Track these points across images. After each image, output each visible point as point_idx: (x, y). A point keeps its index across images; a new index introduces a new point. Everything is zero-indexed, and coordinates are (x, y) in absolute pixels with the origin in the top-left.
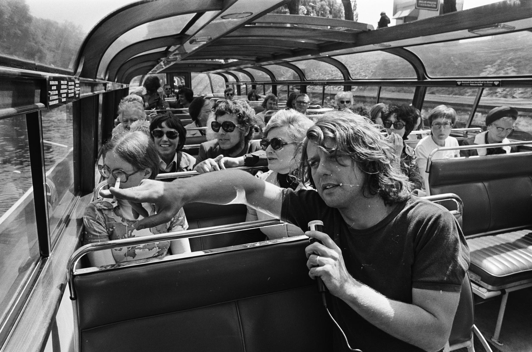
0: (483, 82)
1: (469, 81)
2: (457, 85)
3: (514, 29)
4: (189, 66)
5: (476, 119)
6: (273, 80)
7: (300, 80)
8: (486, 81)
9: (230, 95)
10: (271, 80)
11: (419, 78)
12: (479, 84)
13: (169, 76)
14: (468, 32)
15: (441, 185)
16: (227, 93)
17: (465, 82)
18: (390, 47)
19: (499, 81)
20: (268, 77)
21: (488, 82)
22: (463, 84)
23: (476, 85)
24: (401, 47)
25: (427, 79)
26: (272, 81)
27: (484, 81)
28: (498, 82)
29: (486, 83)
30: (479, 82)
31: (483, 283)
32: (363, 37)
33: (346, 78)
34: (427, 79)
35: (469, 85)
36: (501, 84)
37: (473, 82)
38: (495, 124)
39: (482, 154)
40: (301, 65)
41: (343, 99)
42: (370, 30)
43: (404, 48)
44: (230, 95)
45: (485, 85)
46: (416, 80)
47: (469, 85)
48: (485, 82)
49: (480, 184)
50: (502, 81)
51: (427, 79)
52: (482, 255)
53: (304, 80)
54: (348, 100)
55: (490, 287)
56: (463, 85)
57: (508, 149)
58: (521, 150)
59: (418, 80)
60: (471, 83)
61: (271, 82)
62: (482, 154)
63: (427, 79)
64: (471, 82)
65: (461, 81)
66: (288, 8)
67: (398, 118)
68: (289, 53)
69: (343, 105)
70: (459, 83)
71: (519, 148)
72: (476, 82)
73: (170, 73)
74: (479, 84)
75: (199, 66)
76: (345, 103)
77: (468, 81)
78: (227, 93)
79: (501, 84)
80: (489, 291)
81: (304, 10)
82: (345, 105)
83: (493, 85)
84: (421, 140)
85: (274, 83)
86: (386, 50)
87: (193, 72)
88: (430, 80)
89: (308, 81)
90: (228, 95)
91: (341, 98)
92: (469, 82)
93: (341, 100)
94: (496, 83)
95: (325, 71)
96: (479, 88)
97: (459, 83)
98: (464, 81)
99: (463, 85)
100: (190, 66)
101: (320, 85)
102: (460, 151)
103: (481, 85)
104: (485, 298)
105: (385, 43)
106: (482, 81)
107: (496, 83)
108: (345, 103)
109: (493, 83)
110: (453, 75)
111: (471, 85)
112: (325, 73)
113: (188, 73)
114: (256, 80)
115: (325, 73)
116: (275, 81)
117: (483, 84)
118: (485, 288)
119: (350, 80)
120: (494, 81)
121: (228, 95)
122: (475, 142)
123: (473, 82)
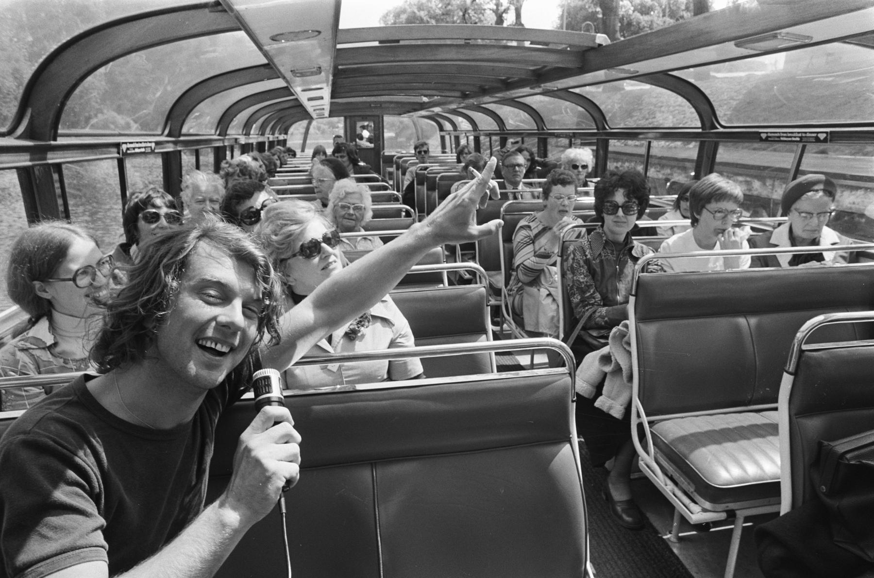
0: (800, 135)
1: (780, 133)
2: (761, 140)
3: (812, 39)
4: (370, 105)
5: (840, 199)
6: (501, 129)
7: (595, 128)
8: (806, 133)
9: (423, 153)
10: (498, 129)
11: (703, 127)
12: (795, 137)
13: (348, 121)
14: (734, 47)
15: (667, 318)
16: (418, 150)
17: (773, 135)
18: (637, 74)
19: (826, 133)
20: (493, 126)
21: (808, 135)
22: (770, 137)
23: (790, 139)
24: (665, 73)
25: (718, 128)
26: (500, 130)
27: (802, 133)
28: (825, 135)
29: (806, 137)
30: (794, 135)
31: (698, 498)
32: (592, 57)
33: (600, 126)
34: (717, 128)
35: (779, 139)
36: (829, 137)
37: (785, 135)
38: (796, 210)
39: (745, 264)
40: (537, 101)
41: (576, 161)
42: (602, 45)
43: (670, 73)
44: (423, 153)
45: (803, 140)
46: (700, 130)
47: (779, 139)
48: (804, 135)
49: (742, 321)
50: (831, 132)
51: (717, 128)
52: (51, 443)
53: (543, 129)
54: (585, 164)
55: (708, 505)
56: (769, 139)
57: (784, 260)
58: (862, 259)
59: (703, 130)
60: (783, 137)
61: (499, 132)
62: (745, 264)
63: (717, 128)
64: (782, 135)
65: (767, 133)
66: (601, 7)
67: (628, 195)
68: (499, 85)
69: (576, 171)
70: (764, 136)
71: (857, 256)
72: (789, 135)
73: (350, 116)
74: (795, 137)
75: (387, 105)
76: (580, 169)
77: (776, 133)
78: (418, 150)
79: (829, 137)
80: (705, 510)
81: (628, 7)
82: (579, 172)
83: (817, 140)
84: (675, 238)
85: (504, 135)
86: (637, 78)
87: (387, 114)
88: (721, 130)
89: (509, 132)
90: (420, 152)
91: (572, 160)
92: (778, 135)
93: (575, 163)
94: (822, 137)
95: (649, 113)
96: (797, 145)
97: (764, 136)
98: (771, 133)
99: (769, 139)
100: (372, 105)
101: (565, 137)
102: (752, 257)
103: (798, 139)
104: (692, 523)
105: (626, 67)
106: (799, 133)
107: (822, 137)
108: (580, 169)
109: (817, 136)
110: (758, 122)
111: (782, 139)
112: (647, 116)
113: (378, 116)
114: (508, 128)
115: (647, 116)
116: (504, 130)
117: (801, 137)
118: (700, 506)
119: (606, 129)
120: (818, 133)
121: (420, 152)
122: (772, 241)
123: (785, 135)
